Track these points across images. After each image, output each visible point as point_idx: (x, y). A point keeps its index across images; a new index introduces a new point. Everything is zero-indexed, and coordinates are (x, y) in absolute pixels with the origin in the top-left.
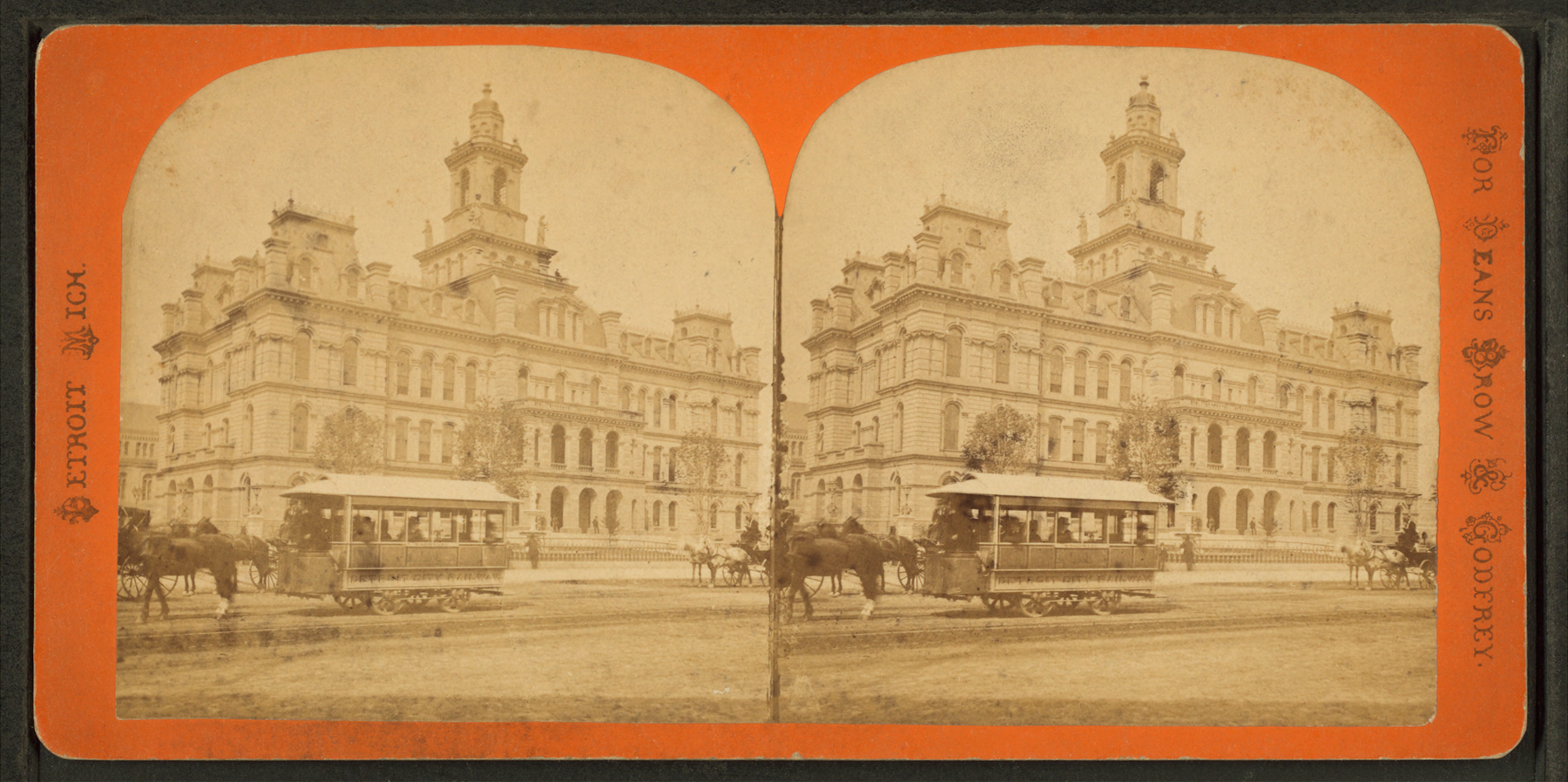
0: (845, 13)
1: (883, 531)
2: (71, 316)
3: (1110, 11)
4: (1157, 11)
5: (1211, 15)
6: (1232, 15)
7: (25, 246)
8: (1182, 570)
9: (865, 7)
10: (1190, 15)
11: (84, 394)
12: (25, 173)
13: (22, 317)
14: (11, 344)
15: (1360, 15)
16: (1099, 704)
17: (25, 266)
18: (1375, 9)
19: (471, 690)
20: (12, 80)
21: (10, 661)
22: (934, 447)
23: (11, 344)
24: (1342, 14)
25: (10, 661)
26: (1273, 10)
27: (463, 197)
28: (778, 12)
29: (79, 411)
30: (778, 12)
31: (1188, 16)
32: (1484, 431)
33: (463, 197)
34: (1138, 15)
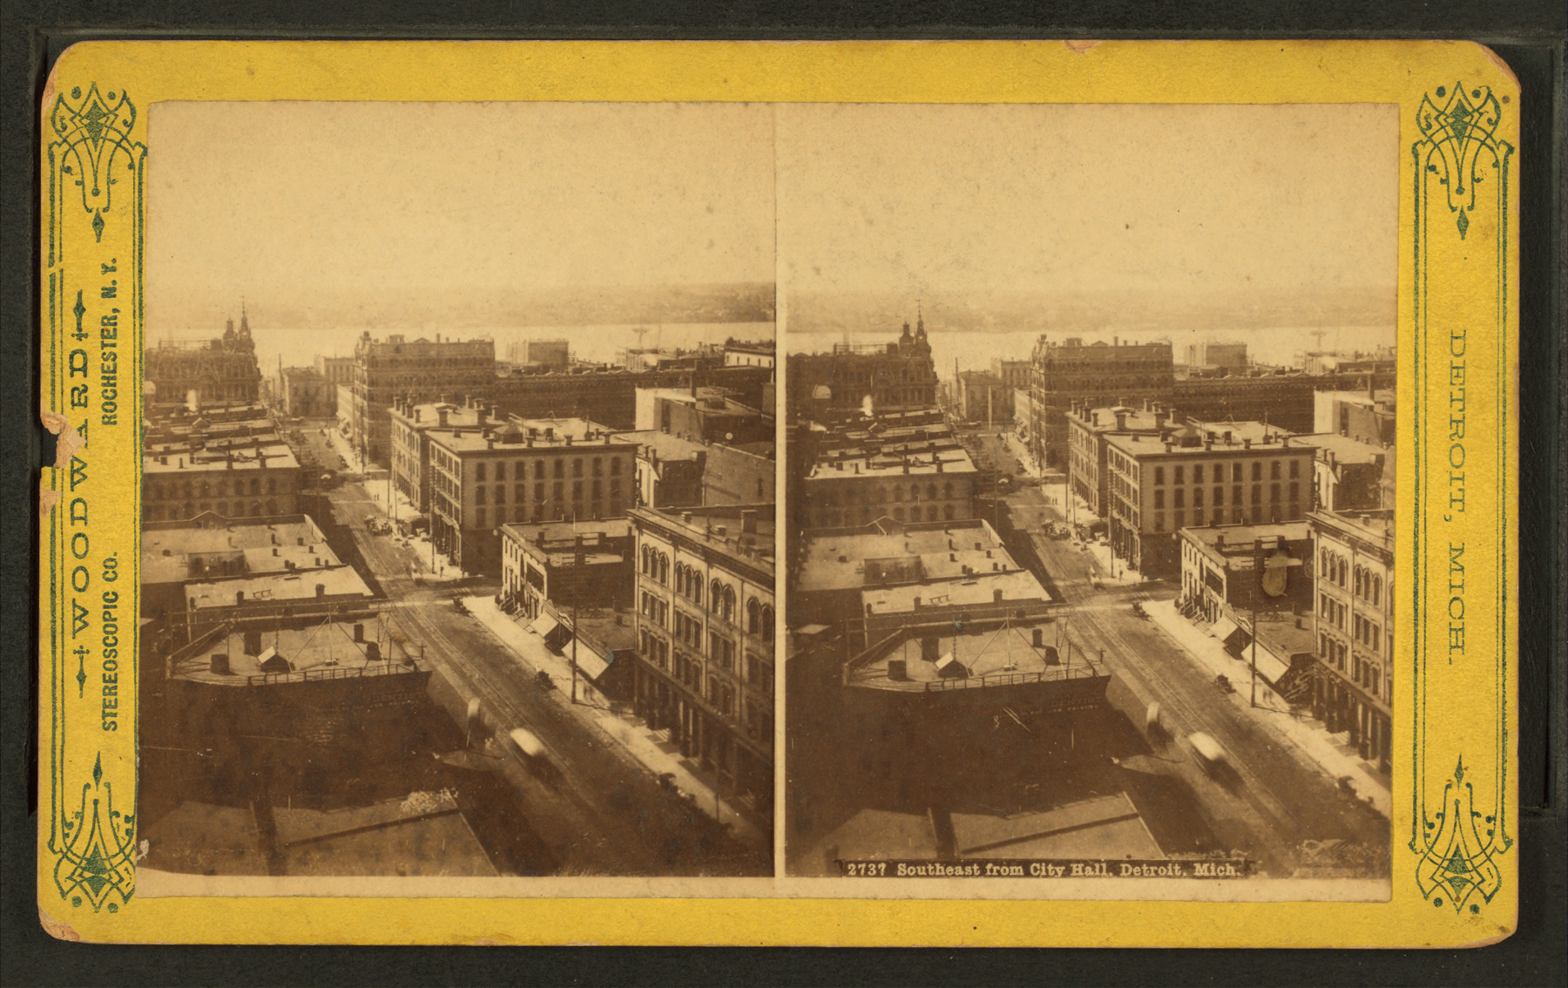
0: (856, 26)
3: (1123, 26)
4: (1171, 27)
5: (1225, 30)
6: (1247, 31)
7: (30, 254)
8: (681, 788)
9: (877, 21)
10: (1204, 30)
12: (31, 181)
13: (26, 326)
14: (15, 353)
15: (1375, 32)
16: (435, 873)
17: (29, 272)
18: (1390, 27)
19: (1355, 883)
20: (18, 88)
22: (81, 854)
23: (15, 353)
26: (1288, 27)
29: (106, 341)
30: (789, 25)
31: (1202, 31)
32: (1072, 649)
34: (1151, 30)
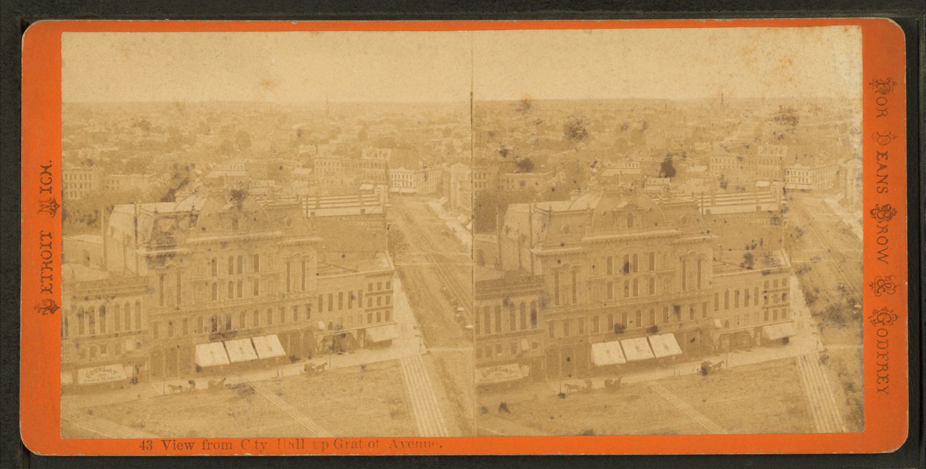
18: (823, 8)
20: (11, 54)
26: (762, 9)
28: (467, 11)
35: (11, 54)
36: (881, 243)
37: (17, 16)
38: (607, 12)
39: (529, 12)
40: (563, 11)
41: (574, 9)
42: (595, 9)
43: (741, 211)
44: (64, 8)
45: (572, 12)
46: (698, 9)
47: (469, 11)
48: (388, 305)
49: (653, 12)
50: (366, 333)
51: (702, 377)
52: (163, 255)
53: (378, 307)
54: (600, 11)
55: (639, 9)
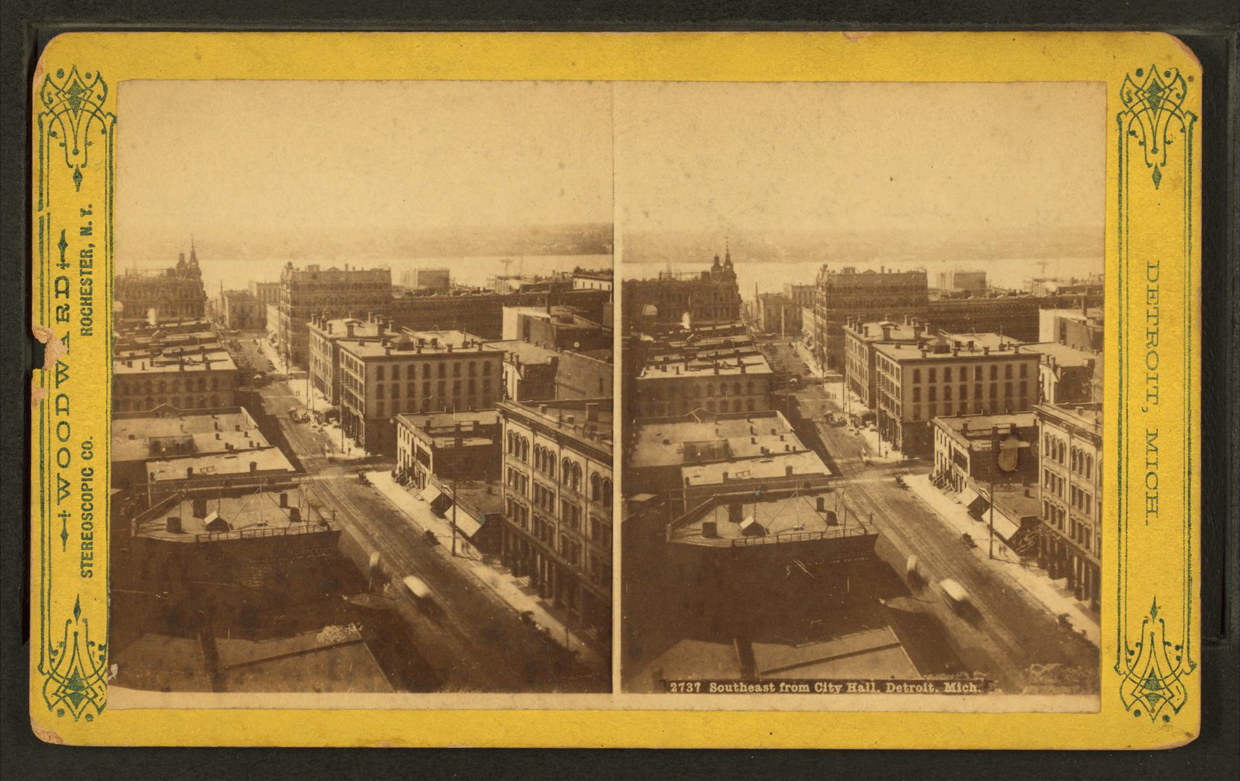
1: (123, 273)
2: (60, 413)
3: (888, 21)
4: (926, 21)
5: (969, 24)
7: (23, 201)
10: (952, 24)
11: (67, 297)
12: (24, 143)
15: (1087, 26)
17: (23, 215)
18: (1099, 21)
20: (14, 69)
21: (10, 531)
24: (1072, 25)
25: (10, 531)
26: (1019, 21)
27: (63, 256)
28: (624, 20)
30: (624, 20)
33: (63, 256)
35: (14, 69)
36: (60, 282)
37: (22, 19)
38: (811, 23)
39: (708, 22)
40: (752, 21)
41: (768, 18)
42: (795, 19)
43: (251, 500)
44: (85, 8)
45: (764, 22)
46: (933, 21)
47: (627, 20)
48: (470, 360)
49: (873, 24)
50: (144, 459)
51: (787, 465)
52: (231, 310)
53: (475, 360)
54: (803, 22)
55: (854, 19)
